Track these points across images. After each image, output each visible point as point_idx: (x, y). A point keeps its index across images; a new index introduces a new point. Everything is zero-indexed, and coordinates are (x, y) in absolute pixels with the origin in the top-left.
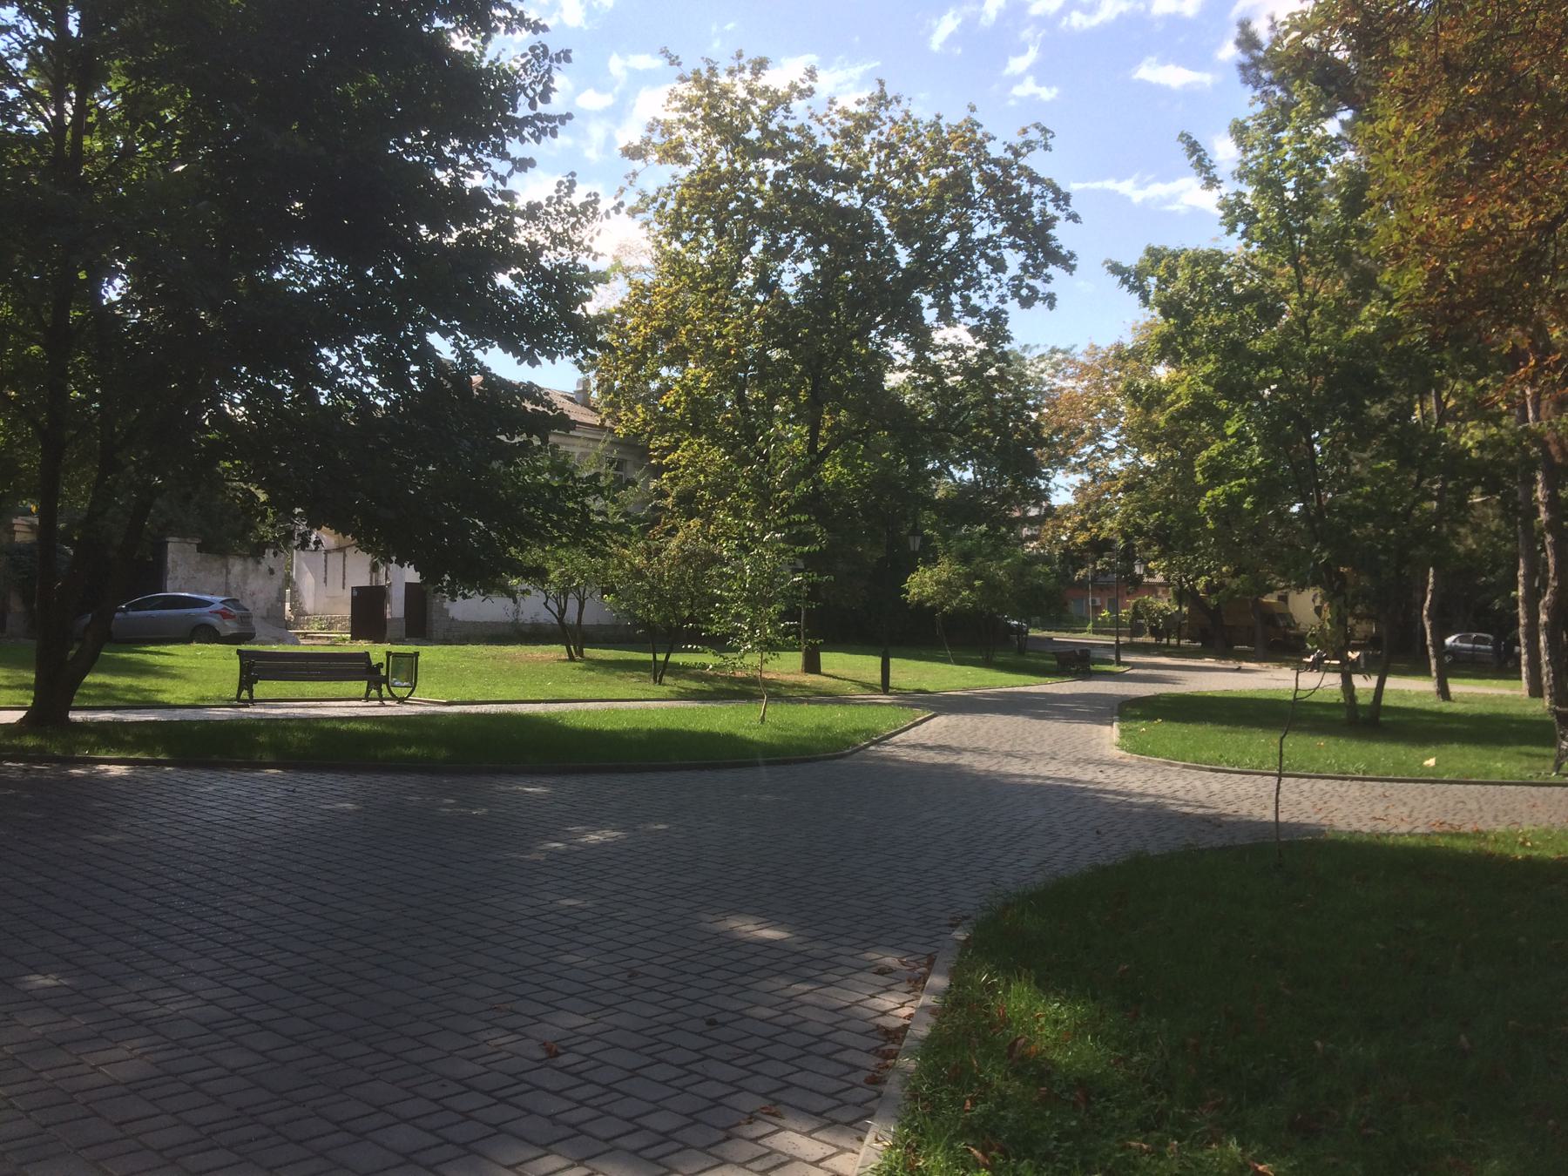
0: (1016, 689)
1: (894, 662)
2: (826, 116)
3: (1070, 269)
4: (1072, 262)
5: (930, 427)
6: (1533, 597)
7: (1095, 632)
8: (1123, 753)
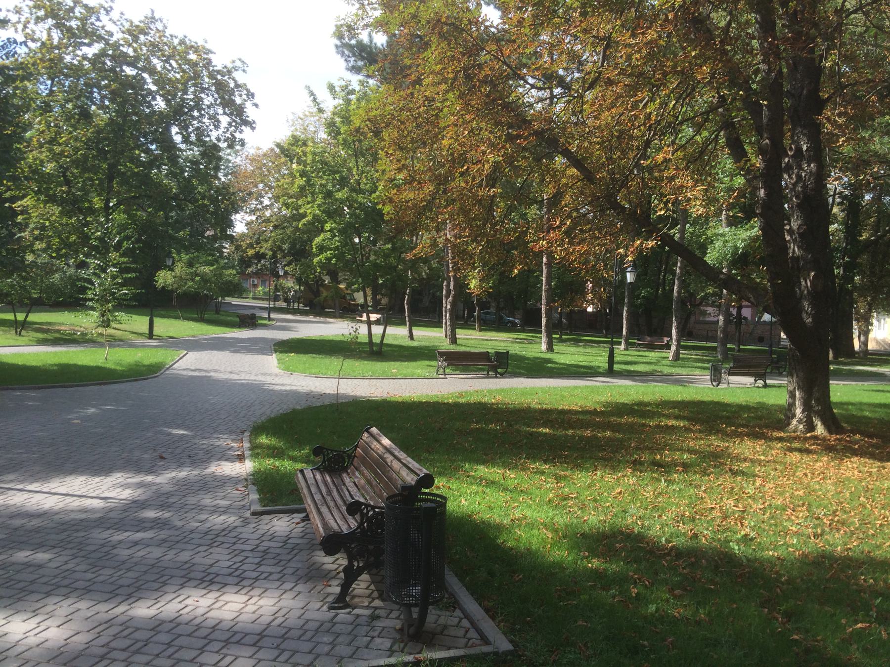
0: (220, 336)
1: (157, 321)
2: (119, 21)
3: (253, 128)
4: (254, 125)
5: (176, 197)
6: (447, 297)
7: (254, 299)
8: (280, 371)
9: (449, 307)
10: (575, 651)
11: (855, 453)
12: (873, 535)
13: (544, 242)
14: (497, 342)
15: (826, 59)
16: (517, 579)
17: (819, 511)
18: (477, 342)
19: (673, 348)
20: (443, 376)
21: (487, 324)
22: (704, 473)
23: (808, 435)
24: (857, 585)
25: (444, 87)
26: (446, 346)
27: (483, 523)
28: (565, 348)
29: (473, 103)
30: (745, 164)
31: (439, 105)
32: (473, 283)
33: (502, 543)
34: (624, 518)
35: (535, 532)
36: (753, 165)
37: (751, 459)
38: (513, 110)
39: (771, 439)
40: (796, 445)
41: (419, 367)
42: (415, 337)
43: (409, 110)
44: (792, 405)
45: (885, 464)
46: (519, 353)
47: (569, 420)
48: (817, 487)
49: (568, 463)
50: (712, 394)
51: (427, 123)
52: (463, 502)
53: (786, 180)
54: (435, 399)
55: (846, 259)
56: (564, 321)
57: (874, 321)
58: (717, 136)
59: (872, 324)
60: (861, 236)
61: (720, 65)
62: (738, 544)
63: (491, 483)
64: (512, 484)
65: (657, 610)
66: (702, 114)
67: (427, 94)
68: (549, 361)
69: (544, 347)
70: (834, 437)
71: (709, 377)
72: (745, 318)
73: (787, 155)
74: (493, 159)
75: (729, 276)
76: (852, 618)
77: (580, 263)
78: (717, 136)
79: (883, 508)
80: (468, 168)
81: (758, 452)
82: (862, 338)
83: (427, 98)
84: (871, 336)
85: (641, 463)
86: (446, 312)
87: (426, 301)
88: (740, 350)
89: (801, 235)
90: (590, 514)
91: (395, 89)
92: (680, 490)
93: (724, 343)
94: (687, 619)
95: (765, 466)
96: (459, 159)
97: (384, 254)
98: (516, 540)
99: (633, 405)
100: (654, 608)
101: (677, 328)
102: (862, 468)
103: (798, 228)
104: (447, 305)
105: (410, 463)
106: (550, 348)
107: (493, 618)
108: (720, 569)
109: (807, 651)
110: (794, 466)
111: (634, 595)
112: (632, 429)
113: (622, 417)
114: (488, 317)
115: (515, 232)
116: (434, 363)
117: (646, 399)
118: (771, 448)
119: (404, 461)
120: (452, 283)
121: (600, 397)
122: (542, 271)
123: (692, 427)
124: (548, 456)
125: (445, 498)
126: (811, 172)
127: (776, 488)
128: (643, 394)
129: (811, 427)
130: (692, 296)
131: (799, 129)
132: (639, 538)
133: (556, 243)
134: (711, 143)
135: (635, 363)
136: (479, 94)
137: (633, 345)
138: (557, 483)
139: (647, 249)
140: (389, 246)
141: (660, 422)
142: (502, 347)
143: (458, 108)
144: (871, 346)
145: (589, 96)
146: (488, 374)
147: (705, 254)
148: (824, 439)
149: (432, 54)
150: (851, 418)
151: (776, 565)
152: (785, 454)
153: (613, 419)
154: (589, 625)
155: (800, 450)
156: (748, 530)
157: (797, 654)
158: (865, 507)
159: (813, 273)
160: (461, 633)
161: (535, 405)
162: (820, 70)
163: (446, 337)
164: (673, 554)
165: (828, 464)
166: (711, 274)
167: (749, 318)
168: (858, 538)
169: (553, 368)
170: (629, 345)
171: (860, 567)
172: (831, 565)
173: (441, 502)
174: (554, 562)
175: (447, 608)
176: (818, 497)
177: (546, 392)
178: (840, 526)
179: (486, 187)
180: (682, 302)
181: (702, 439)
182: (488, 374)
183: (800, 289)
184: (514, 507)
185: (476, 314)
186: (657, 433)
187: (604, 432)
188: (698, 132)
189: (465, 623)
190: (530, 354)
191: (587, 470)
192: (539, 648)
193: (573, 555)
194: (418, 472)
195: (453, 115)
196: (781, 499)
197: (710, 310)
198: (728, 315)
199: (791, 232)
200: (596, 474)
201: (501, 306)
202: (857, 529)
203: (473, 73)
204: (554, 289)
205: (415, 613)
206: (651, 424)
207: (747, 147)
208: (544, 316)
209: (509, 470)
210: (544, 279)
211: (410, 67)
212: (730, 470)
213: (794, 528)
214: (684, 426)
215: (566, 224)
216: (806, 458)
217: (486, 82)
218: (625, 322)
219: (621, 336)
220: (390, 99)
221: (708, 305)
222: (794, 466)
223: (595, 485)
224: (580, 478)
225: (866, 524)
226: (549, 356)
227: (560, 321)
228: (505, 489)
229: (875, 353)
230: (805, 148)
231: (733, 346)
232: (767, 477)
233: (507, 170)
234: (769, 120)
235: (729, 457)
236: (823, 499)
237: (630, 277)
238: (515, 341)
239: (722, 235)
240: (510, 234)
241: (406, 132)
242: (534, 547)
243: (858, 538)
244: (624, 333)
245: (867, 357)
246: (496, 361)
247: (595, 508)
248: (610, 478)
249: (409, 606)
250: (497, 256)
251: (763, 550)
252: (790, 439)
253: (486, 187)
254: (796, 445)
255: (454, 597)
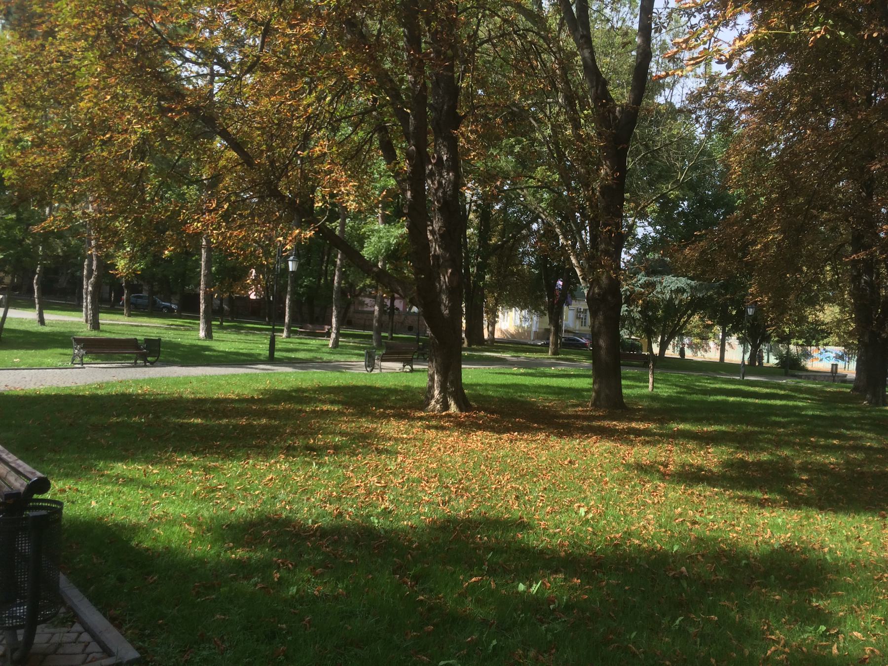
9: (90, 288)
10: (210, 647)
11: (480, 427)
12: (489, 498)
13: (199, 225)
14: (148, 329)
15: (462, 80)
16: (151, 581)
17: (448, 480)
18: (124, 328)
19: (333, 336)
20: (80, 366)
21: (136, 309)
22: (353, 454)
23: (444, 413)
24: (474, 543)
25: (82, 43)
26: (86, 331)
27: (116, 525)
28: (225, 336)
29: (117, 66)
30: (395, 166)
31: (77, 63)
32: (121, 264)
33: (137, 545)
34: (274, 504)
35: (177, 529)
36: (401, 168)
37: (395, 438)
38: (163, 80)
39: (413, 419)
40: (434, 423)
41: (50, 356)
42: (46, 322)
43: (38, 63)
44: (431, 388)
45: (501, 436)
46: (174, 340)
47: (224, 409)
48: (448, 459)
49: (219, 454)
50: (366, 379)
51: (61, 81)
52: (94, 504)
53: (429, 184)
54: (68, 392)
55: (479, 260)
56: (226, 307)
57: (500, 314)
58: (371, 137)
59: (498, 317)
60: (491, 240)
61: (368, 69)
62: (378, 518)
63: (129, 481)
64: (153, 481)
65: (298, 590)
66: (358, 114)
67: (62, 48)
68: (207, 348)
69: (202, 334)
70: (464, 414)
71: (363, 363)
72: (397, 309)
73: (431, 163)
74: (141, 130)
75: (383, 271)
76: (469, 574)
77: (237, 248)
78: (371, 137)
79: (498, 474)
80: (111, 137)
81: (402, 431)
82: (490, 328)
83: (61, 53)
84: (497, 326)
85: (295, 449)
86: (87, 294)
87: (63, 282)
88: (392, 338)
89: (441, 236)
90: (239, 503)
91: (20, 38)
92: (330, 471)
93: (378, 333)
94: (326, 595)
95: (406, 443)
96: (99, 126)
97: (6, 225)
98: (154, 539)
99: (291, 391)
100: (295, 590)
101: (337, 317)
102: (484, 440)
103: (439, 230)
104: (88, 286)
105: (20, 466)
106: (209, 335)
107: (119, 627)
108: (360, 543)
109: (431, 609)
110: (431, 442)
111: (276, 580)
112: (288, 415)
113: (279, 403)
114: (140, 301)
115: (166, 211)
116: (69, 351)
117: (305, 385)
118: (413, 427)
119: (13, 465)
120: (95, 263)
121: (258, 385)
122: (201, 255)
123: (345, 411)
124: (198, 447)
125: (60, 504)
126: (450, 180)
127: (414, 462)
128: (303, 380)
129: (446, 407)
130: (352, 286)
131: (440, 141)
132: (288, 522)
133: (211, 226)
134: (366, 143)
135: (296, 350)
136: (125, 58)
137: (296, 332)
138: (206, 475)
139: (306, 239)
140: (14, 216)
141: (316, 407)
142: (153, 334)
143: (99, 69)
144: (497, 335)
145: (249, 79)
146: (136, 363)
147: (363, 247)
148: (456, 417)
149: (67, 5)
150: (479, 398)
151: (409, 533)
152: (424, 432)
153: (270, 406)
154: (227, 618)
155: (436, 428)
156: (387, 504)
157: (421, 614)
158: (484, 474)
159: (450, 271)
160: (79, 648)
161: (188, 395)
162: (458, 89)
163: (87, 321)
164: (318, 534)
165: (458, 438)
166: (366, 267)
167: (401, 309)
168: (477, 502)
169: (211, 356)
170: (291, 333)
171: (477, 527)
172: (455, 528)
173: (56, 508)
174: (194, 558)
175: (63, 623)
176: (448, 468)
177: (202, 381)
178: (463, 492)
179: (132, 159)
180: (343, 292)
181: (353, 421)
182: (136, 363)
183: (440, 284)
184: (155, 505)
185: (124, 297)
186: (312, 418)
187: (260, 419)
188: (354, 131)
189: (86, 637)
190: (186, 341)
191: (239, 459)
192: (171, 649)
193: (216, 548)
194: (30, 476)
195: (92, 75)
196: (418, 473)
197: (367, 300)
198: (382, 306)
199: (433, 232)
200: (248, 463)
201: (156, 289)
202: (477, 494)
203: (118, 34)
204: (215, 274)
205: (21, 635)
206: (308, 409)
207: (397, 152)
208: (202, 301)
209: (152, 465)
210: (203, 264)
211: (41, 16)
212: (377, 449)
213: (426, 498)
214: (338, 410)
215: (223, 207)
216: (440, 434)
217: (133, 47)
218: (287, 310)
219: (283, 323)
220: (14, 48)
221: (365, 296)
222: (431, 442)
223: (247, 474)
224: (231, 468)
225: (484, 489)
226: (207, 343)
227: (221, 307)
228: (145, 486)
229: (500, 341)
230: (445, 158)
231: (386, 335)
232: (407, 453)
233: (158, 143)
234: (415, 128)
235: (376, 437)
236: (452, 470)
237: (292, 266)
238: (169, 328)
239: (378, 231)
240: (160, 213)
241: (34, 88)
242: (173, 545)
243: (477, 502)
244: (287, 320)
245: (494, 344)
246: (145, 349)
247: (244, 498)
248: (262, 466)
249: (14, 629)
250: (145, 235)
251: (399, 521)
252: (428, 418)
253: (132, 159)
254: (434, 423)
255: (74, 611)
